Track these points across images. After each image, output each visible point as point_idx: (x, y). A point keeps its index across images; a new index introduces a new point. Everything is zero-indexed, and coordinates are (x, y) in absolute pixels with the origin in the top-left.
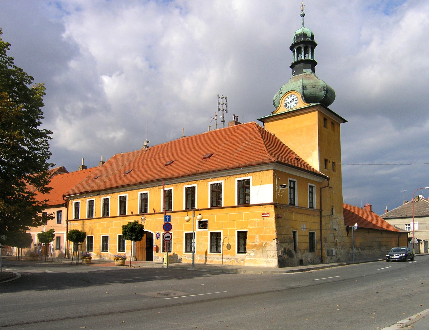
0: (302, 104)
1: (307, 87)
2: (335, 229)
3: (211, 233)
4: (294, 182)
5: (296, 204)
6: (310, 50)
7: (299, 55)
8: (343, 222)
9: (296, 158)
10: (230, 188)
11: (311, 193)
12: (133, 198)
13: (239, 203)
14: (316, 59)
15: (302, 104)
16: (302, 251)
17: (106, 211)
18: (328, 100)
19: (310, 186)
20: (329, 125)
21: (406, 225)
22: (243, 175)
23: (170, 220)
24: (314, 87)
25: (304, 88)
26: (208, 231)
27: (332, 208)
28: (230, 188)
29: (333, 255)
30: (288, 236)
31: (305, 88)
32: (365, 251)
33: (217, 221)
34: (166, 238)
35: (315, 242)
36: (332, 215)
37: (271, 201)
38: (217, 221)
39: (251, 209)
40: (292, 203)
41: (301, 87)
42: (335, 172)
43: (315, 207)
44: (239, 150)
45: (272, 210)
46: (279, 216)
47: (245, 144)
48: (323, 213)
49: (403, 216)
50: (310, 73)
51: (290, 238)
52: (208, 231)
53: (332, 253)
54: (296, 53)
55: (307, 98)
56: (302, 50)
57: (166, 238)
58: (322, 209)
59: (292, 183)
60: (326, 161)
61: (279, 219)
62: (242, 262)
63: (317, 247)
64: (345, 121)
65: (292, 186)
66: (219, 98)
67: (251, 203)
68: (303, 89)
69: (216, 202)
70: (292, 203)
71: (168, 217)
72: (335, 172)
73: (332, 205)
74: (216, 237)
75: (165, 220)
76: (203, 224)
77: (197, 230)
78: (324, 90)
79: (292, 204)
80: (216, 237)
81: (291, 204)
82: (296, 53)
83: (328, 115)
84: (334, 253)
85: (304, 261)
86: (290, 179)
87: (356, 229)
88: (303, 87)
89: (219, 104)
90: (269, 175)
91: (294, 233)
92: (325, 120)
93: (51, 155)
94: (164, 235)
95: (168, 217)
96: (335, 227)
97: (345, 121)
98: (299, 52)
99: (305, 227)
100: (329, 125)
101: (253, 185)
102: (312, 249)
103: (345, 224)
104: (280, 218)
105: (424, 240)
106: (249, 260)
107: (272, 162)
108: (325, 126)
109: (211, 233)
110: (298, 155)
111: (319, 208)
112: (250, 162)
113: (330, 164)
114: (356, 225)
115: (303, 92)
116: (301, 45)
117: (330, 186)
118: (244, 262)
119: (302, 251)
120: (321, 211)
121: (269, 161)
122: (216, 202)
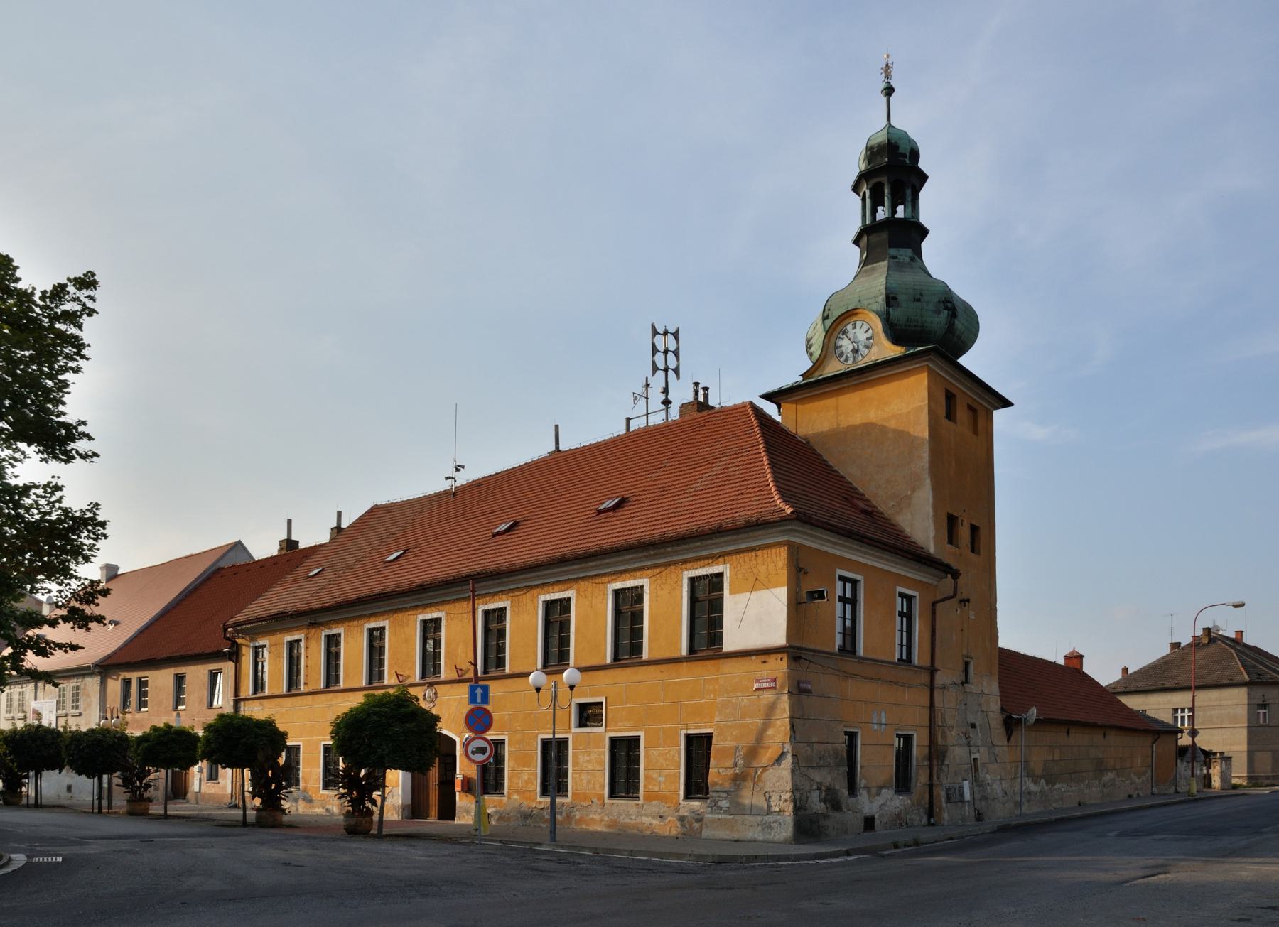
0: (894, 351)
1: (900, 297)
2: (973, 726)
3: (614, 741)
4: (854, 583)
5: (861, 651)
6: (909, 192)
7: (880, 208)
8: (995, 705)
9: (864, 512)
10: (665, 602)
11: (907, 615)
12: (402, 636)
13: (692, 650)
14: (924, 219)
15: (894, 351)
16: (874, 791)
17: (623, 767)
18: (959, 337)
19: (902, 595)
20: (962, 414)
21: (1175, 710)
22: (695, 564)
23: (485, 699)
24: (919, 300)
25: (891, 299)
26: (601, 734)
27: (967, 664)
28: (665, 602)
29: (963, 801)
30: (829, 746)
31: (892, 302)
32: (1057, 786)
33: (633, 703)
34: (473, 753)
35: (914, 763)
36: (967, 681)
37: (780, 639)
38: (633, 703)
39: (729, 667)
40: (848, 647)
41: (882, 299)
42: (979, 554)
43: (916, 660)
44: (700, 485)
45: (779, 666)
46: (803, 686)
47: (717, 468)
48: (940, 679)
49: (1168, 685)
50: (907, 260)
51: (836, 752)
52: (601, 734)
53: (962, 795)
54: (868, 201)
55: (896, 333)
56: (886, 191)
57: (473, 753)
58: (937, 665)
59: (848, 586)
60: (952, 520)
61: (803, 697)
62: (696, 825)
63: (920, 779)
64: (1006, 403)
65: (848, 595)
66: (655, 332)
67: (728, 645)
68: (888, 304)
69: (628, 645)
70: (848, 647)
71: (479, 691)
72: (979, 554)
73: (965, 652)
74: (624, 755)
75: (473, 698)
76: (588, 714)
77: (572, 732)
78: (947, 308)
79: (849, 647)
80: (624, 755)
81: (901, 660)
82: (868, 201)
83: (959, 386)
84: (967, 796)
85: (877, 822)
86: (840, 572)
87: (1032, 721)
88: (887, 297)
89: (655, 350)
90: (776, 561)
91: (852, 737)
92: (950, 397)
93: (58, 488)
94: (466, 745)
95: (479, 691)
96: (971, 719)
97: (1006, 403)
98: (877, 201)
99: (883, 721)
100: (962, 414)
101: (732, 592)
102: (903, 783)
103: (1002, 709)
104: (808, 692)
105: (1222, 753)
106: (713, 821)
107: (785, 520)
108: (950, 415)
109: (614, 741)
110: (874, 503)
111: (928, 664)
112: (722, 519)
113: (964, 533)
114: (1034, 710)
115: (888, 313)
116: (884, 179)
117: (959, 596)
118: (701, 827)
119: (874, 791)
120: (932, 671)
121: (776, 517)
122: (628, 645)
